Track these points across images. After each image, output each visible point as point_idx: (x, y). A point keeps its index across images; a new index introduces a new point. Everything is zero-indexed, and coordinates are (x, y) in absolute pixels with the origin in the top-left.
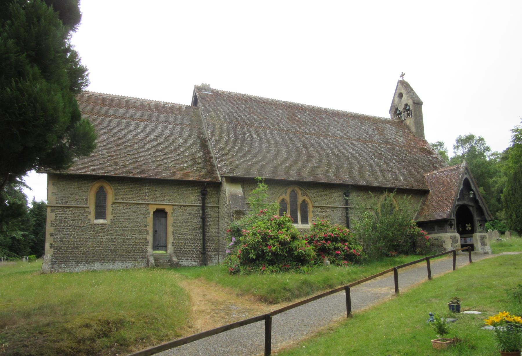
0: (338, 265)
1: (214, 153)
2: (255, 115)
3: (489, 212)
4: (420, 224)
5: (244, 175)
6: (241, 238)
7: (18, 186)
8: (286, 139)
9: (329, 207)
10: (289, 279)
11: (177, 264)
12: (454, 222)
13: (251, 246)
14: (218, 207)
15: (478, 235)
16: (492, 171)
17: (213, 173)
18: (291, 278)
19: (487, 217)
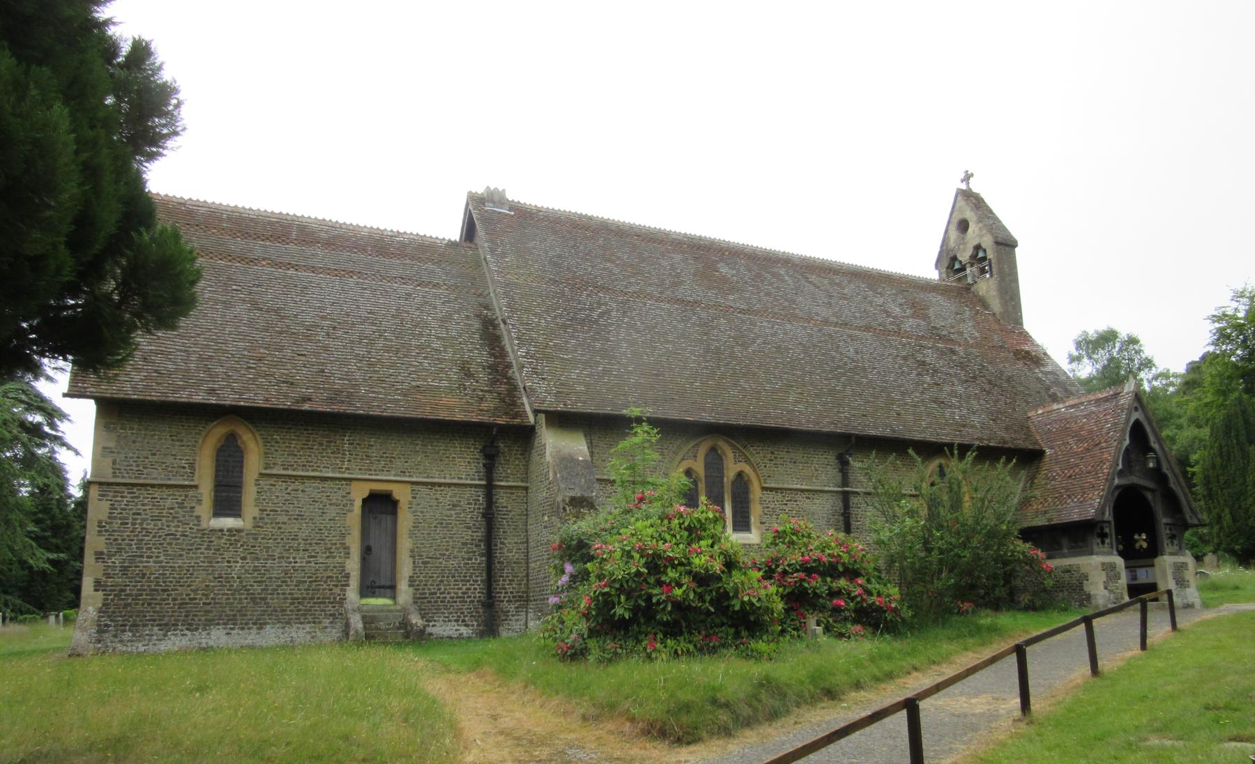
0: (841, 635)
1: (516, 352)
2: (617, 265)
4: (1029, 534)
5: (590, 409)
6: (589, 565)
7: (45, 446)
8: (694, 324)
9: (802, 491)
10: (726, 673)
11: (422, 632)
13: (617, 586)
14: (526, 488)
15: (1167, 561)
16: (1160, 414)
17: (514, 404)
18: (727, 672)
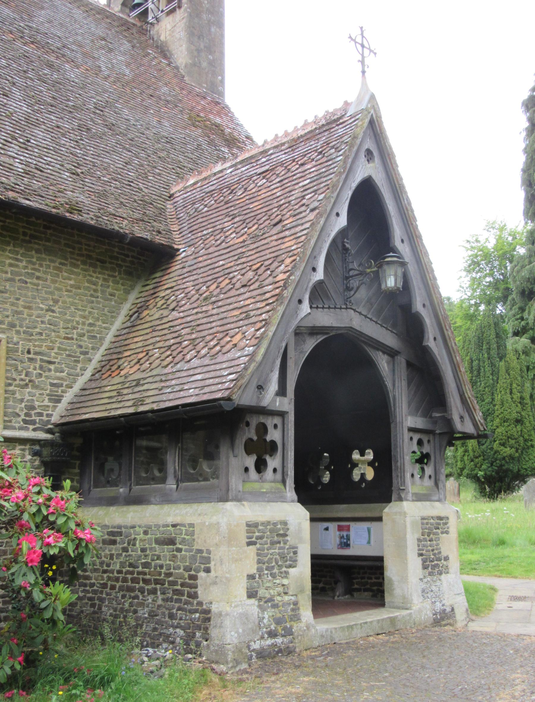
3: (469, 393)
12: (283, 434)
15: (407, 514)
19: (456, 418)
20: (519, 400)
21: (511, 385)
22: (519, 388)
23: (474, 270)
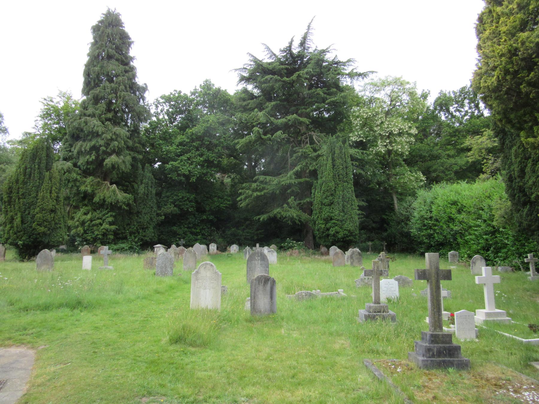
20: (55, 198)
21: (51, 188)
22: (57, 190)
23: (46, 118)
